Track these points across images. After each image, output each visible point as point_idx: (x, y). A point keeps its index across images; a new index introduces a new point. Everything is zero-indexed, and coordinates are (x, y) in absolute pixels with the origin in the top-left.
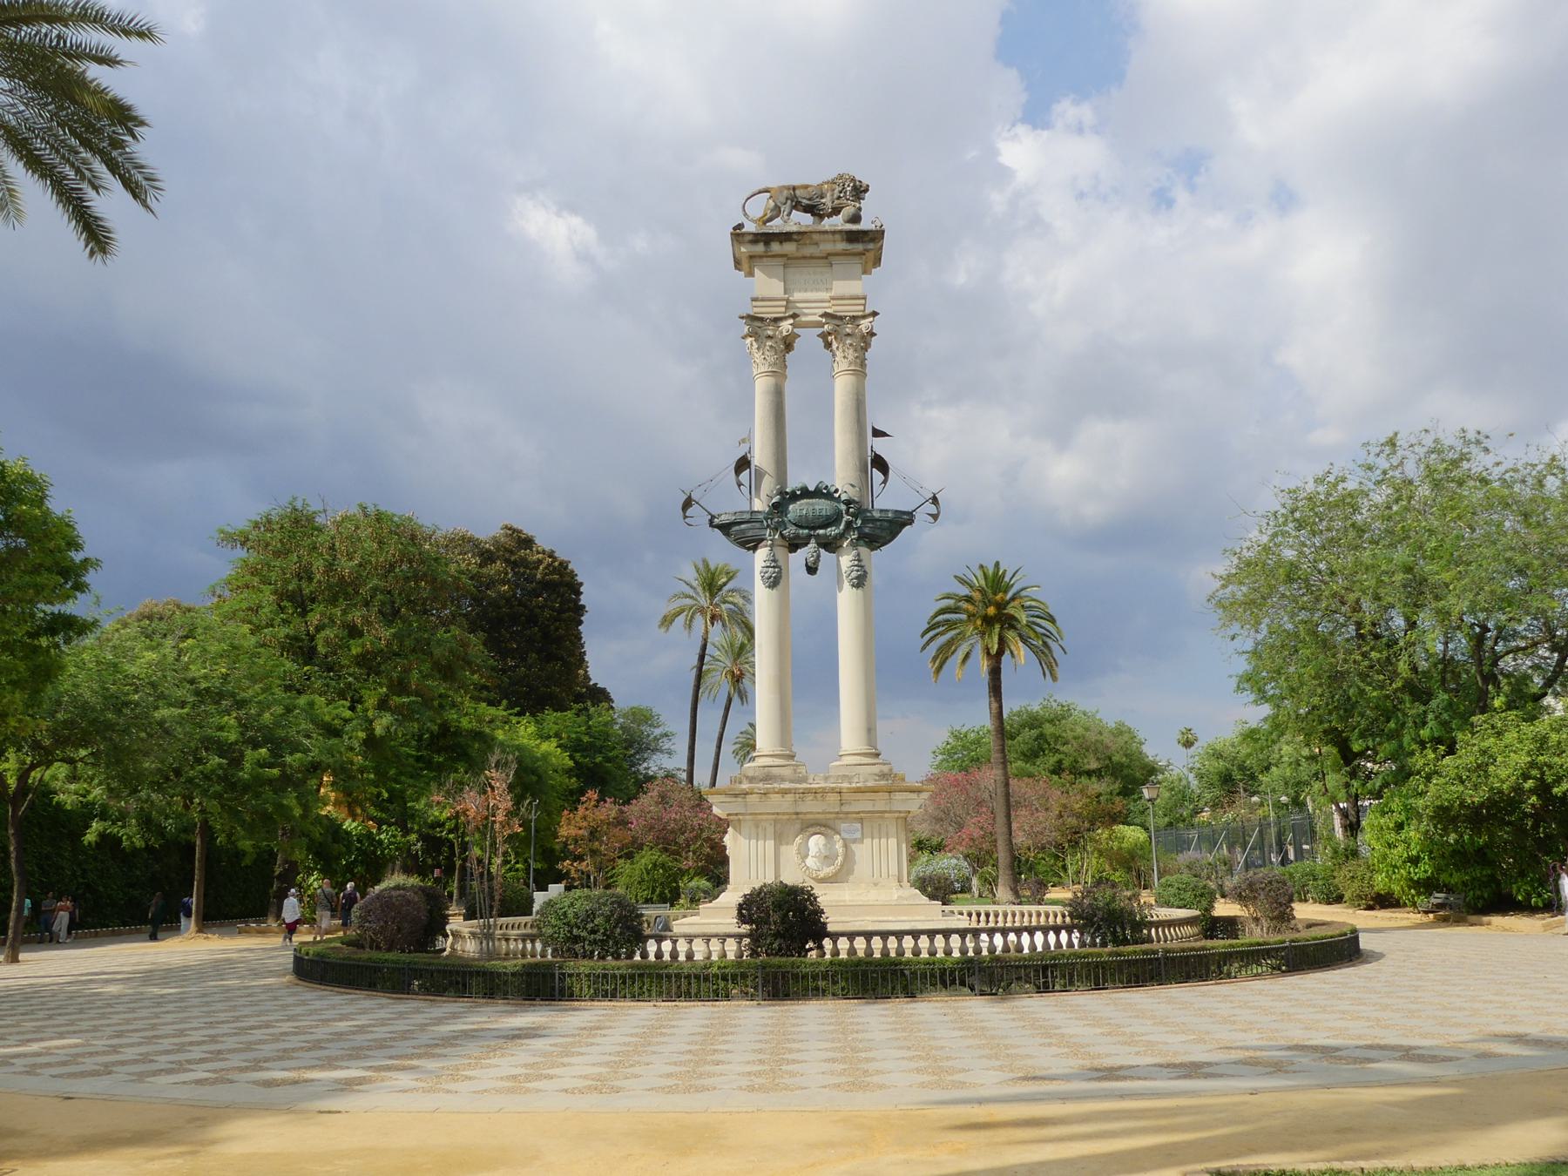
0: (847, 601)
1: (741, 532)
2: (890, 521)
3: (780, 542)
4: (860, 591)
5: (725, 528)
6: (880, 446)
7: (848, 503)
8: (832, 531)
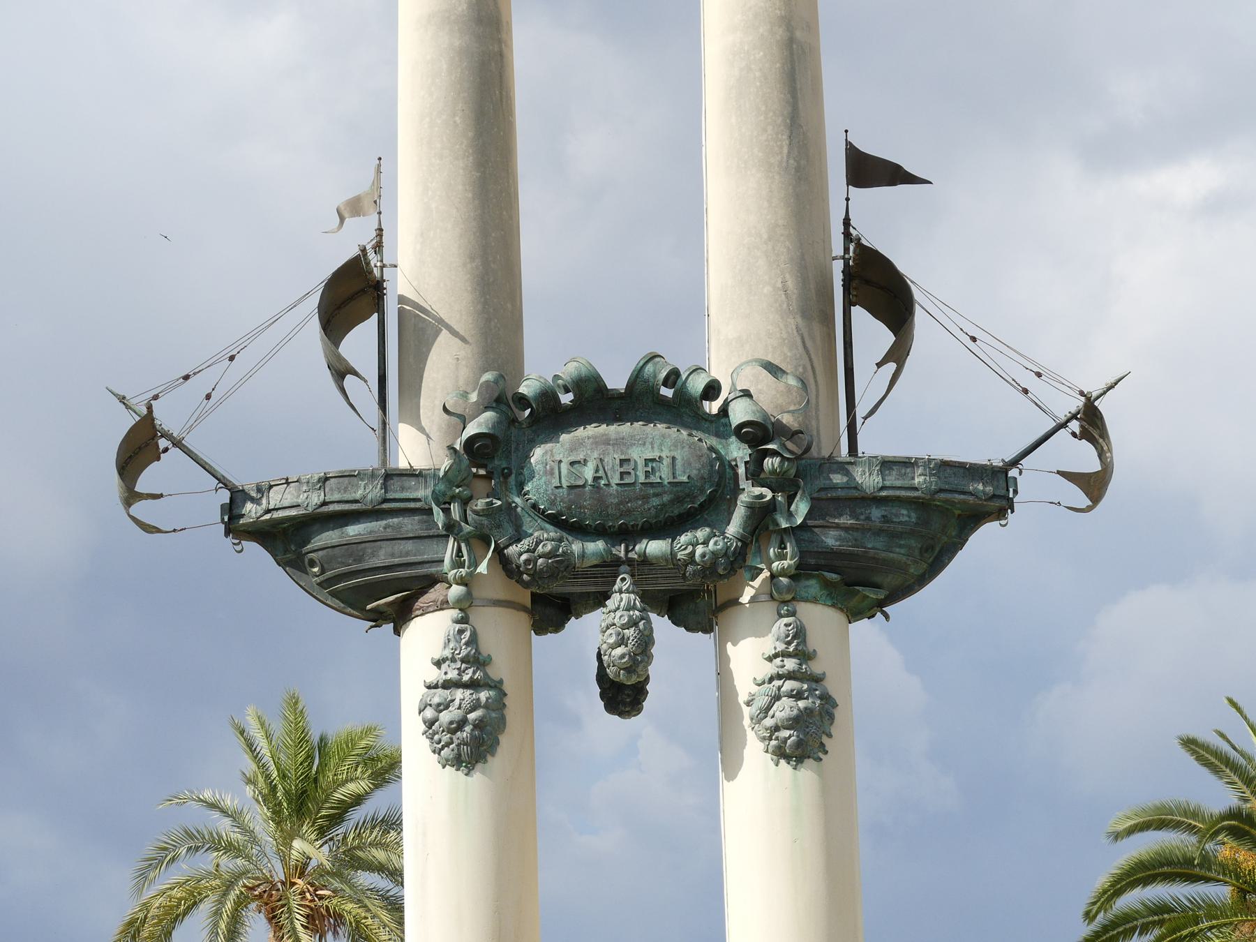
0: (759, 806)
1: (346, 554)
2: (921, 505)
3: (499, 587)
4: (807, 774)
5: (286, 539)
6: (881, 219)
7: (758, 434)
8: (698, 544)
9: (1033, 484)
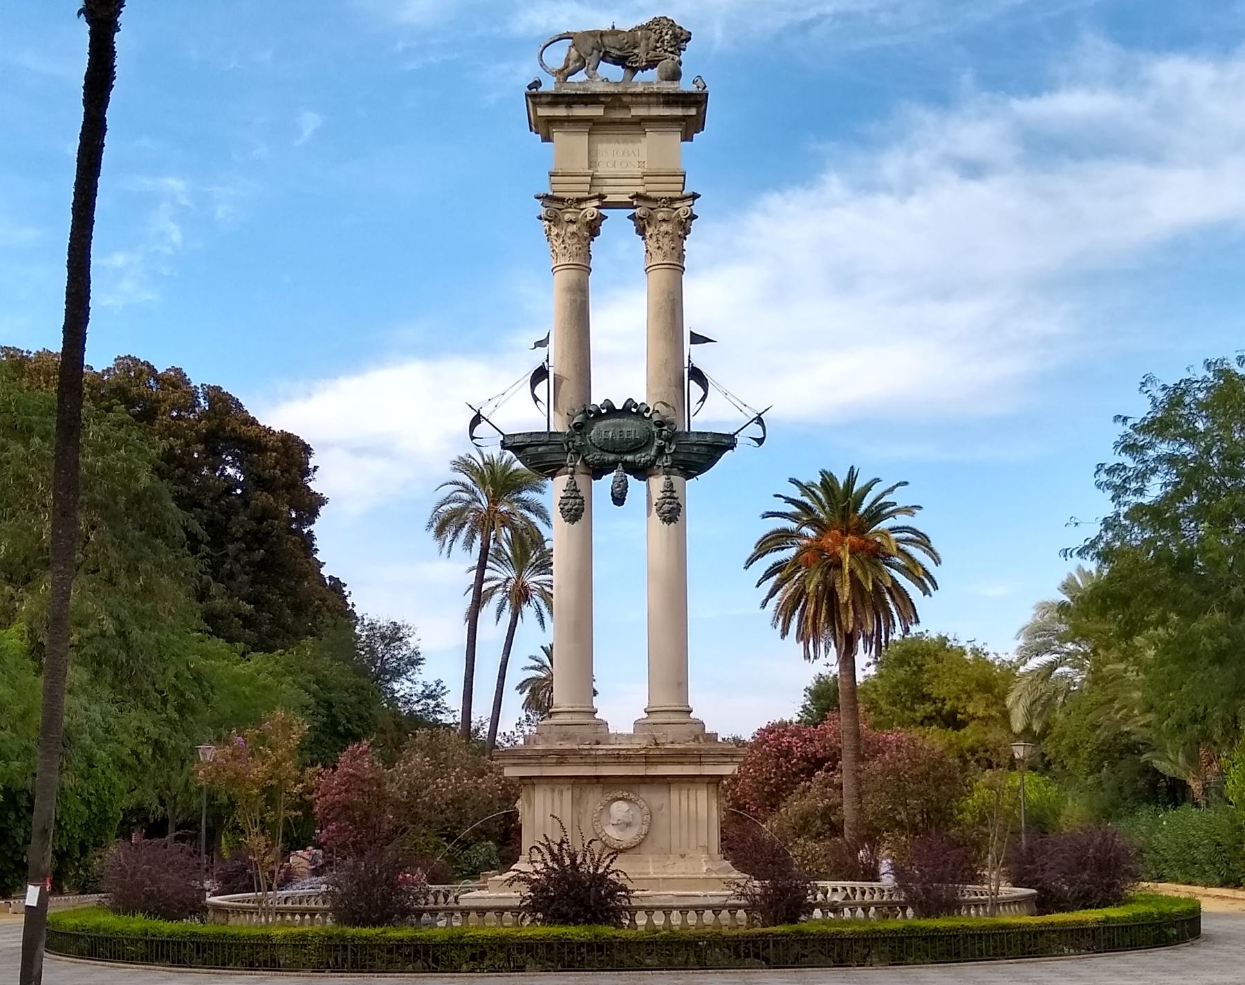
6: (698, 355)
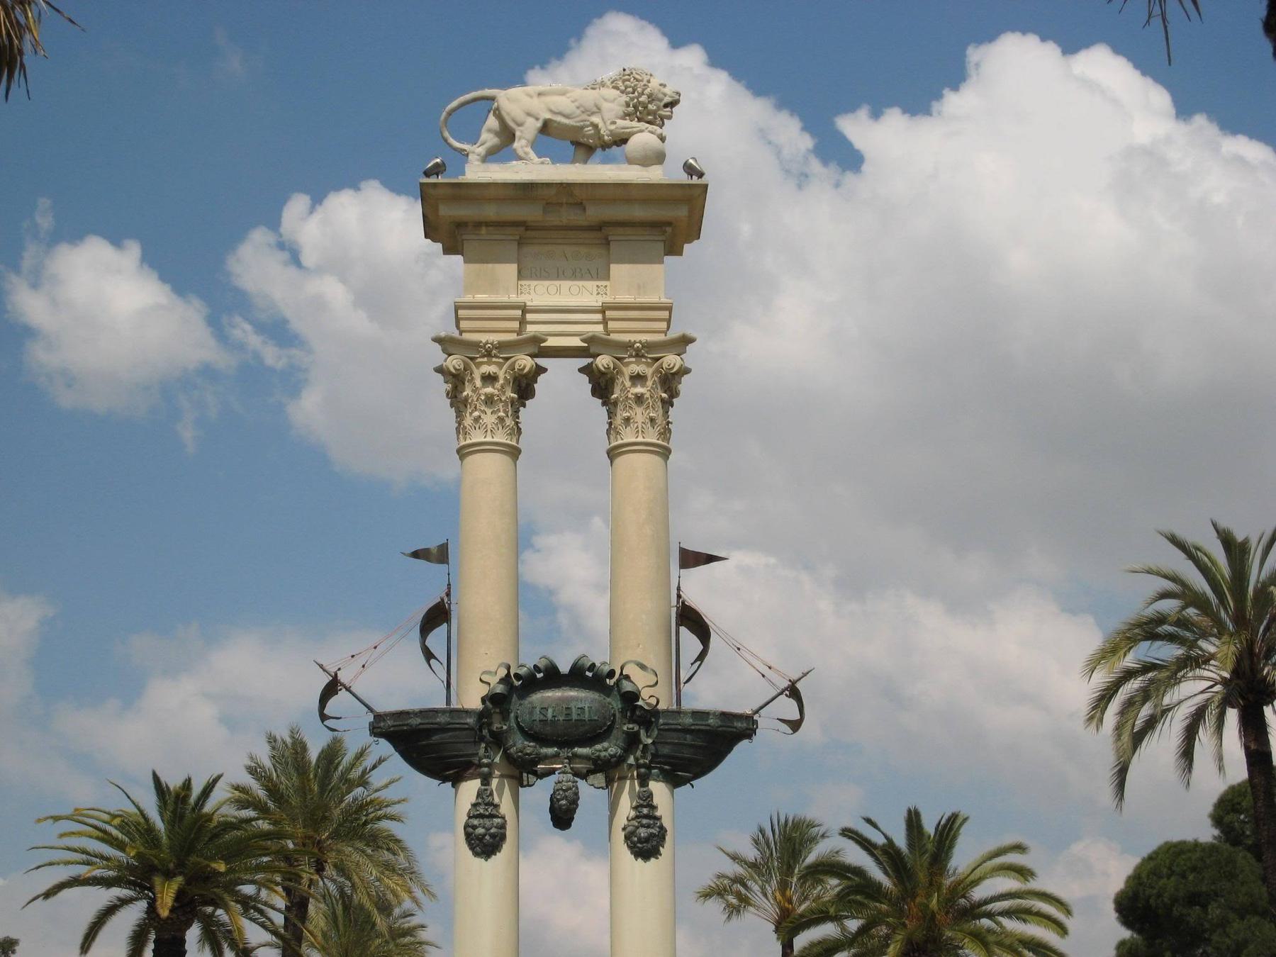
6: (698, 587)
9: (763, 721)
